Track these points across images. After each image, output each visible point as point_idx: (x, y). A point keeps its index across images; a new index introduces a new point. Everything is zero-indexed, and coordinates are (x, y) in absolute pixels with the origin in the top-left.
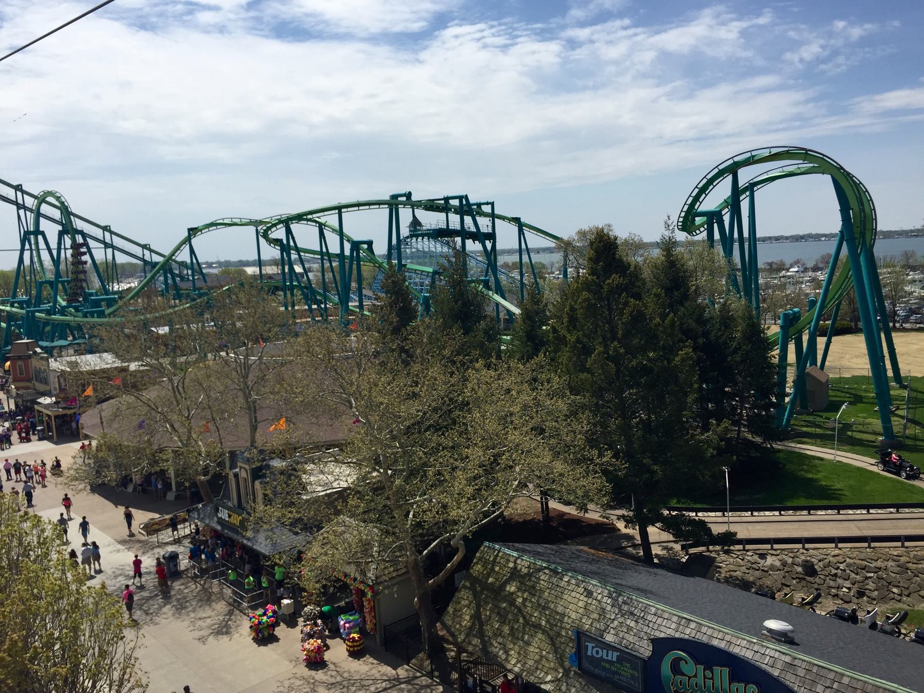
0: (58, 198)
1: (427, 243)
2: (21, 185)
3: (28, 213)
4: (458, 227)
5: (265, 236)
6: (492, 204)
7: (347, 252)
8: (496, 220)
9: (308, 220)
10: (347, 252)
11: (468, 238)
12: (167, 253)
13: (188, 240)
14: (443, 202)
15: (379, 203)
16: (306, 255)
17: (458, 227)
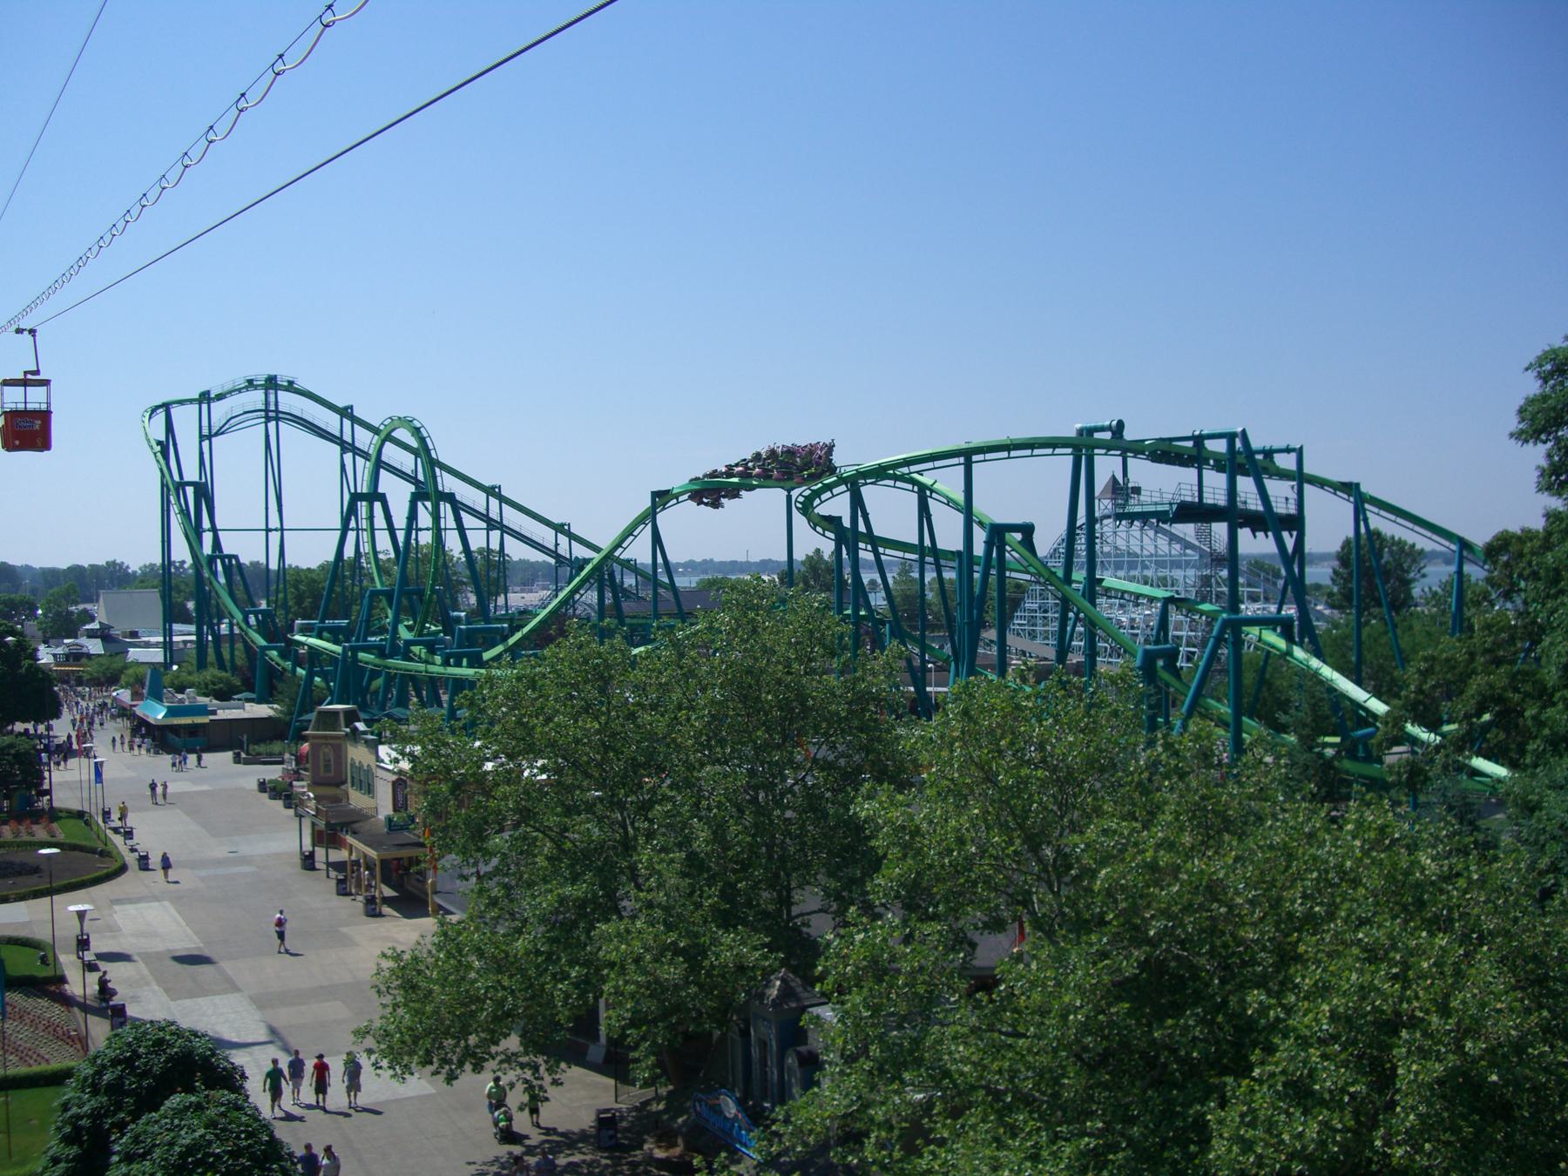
0: (416, 431)
1: (1137, 534)
2: (351, 407)
3: (360, 461)
4: (1222, 500)
5: (807, 508)
6: (1300, 452)
7: (979, 549)
8: (1307, 487)
9: (896, 478)
10: (979, 549)
11: (1242, 526)
12: (605, 544)
13: (650, 516)
14: (1190, 444)
15: (1053, 444)
16: (888, 551)
17: (1222, 500)
